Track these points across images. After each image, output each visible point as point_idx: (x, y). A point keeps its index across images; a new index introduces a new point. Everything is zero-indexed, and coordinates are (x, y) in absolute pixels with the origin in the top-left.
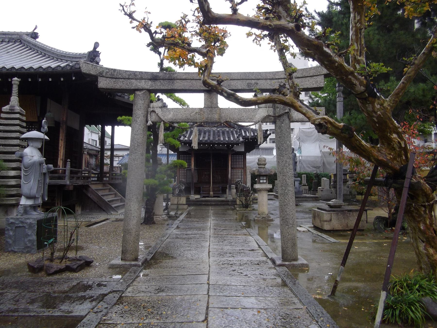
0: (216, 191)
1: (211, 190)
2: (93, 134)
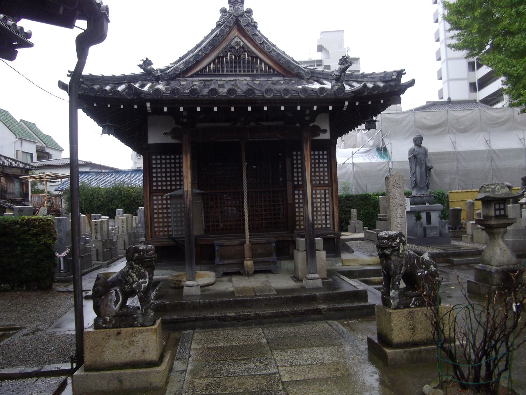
0: (261, 255)
1: (247, 253)
2: (25, 144)
